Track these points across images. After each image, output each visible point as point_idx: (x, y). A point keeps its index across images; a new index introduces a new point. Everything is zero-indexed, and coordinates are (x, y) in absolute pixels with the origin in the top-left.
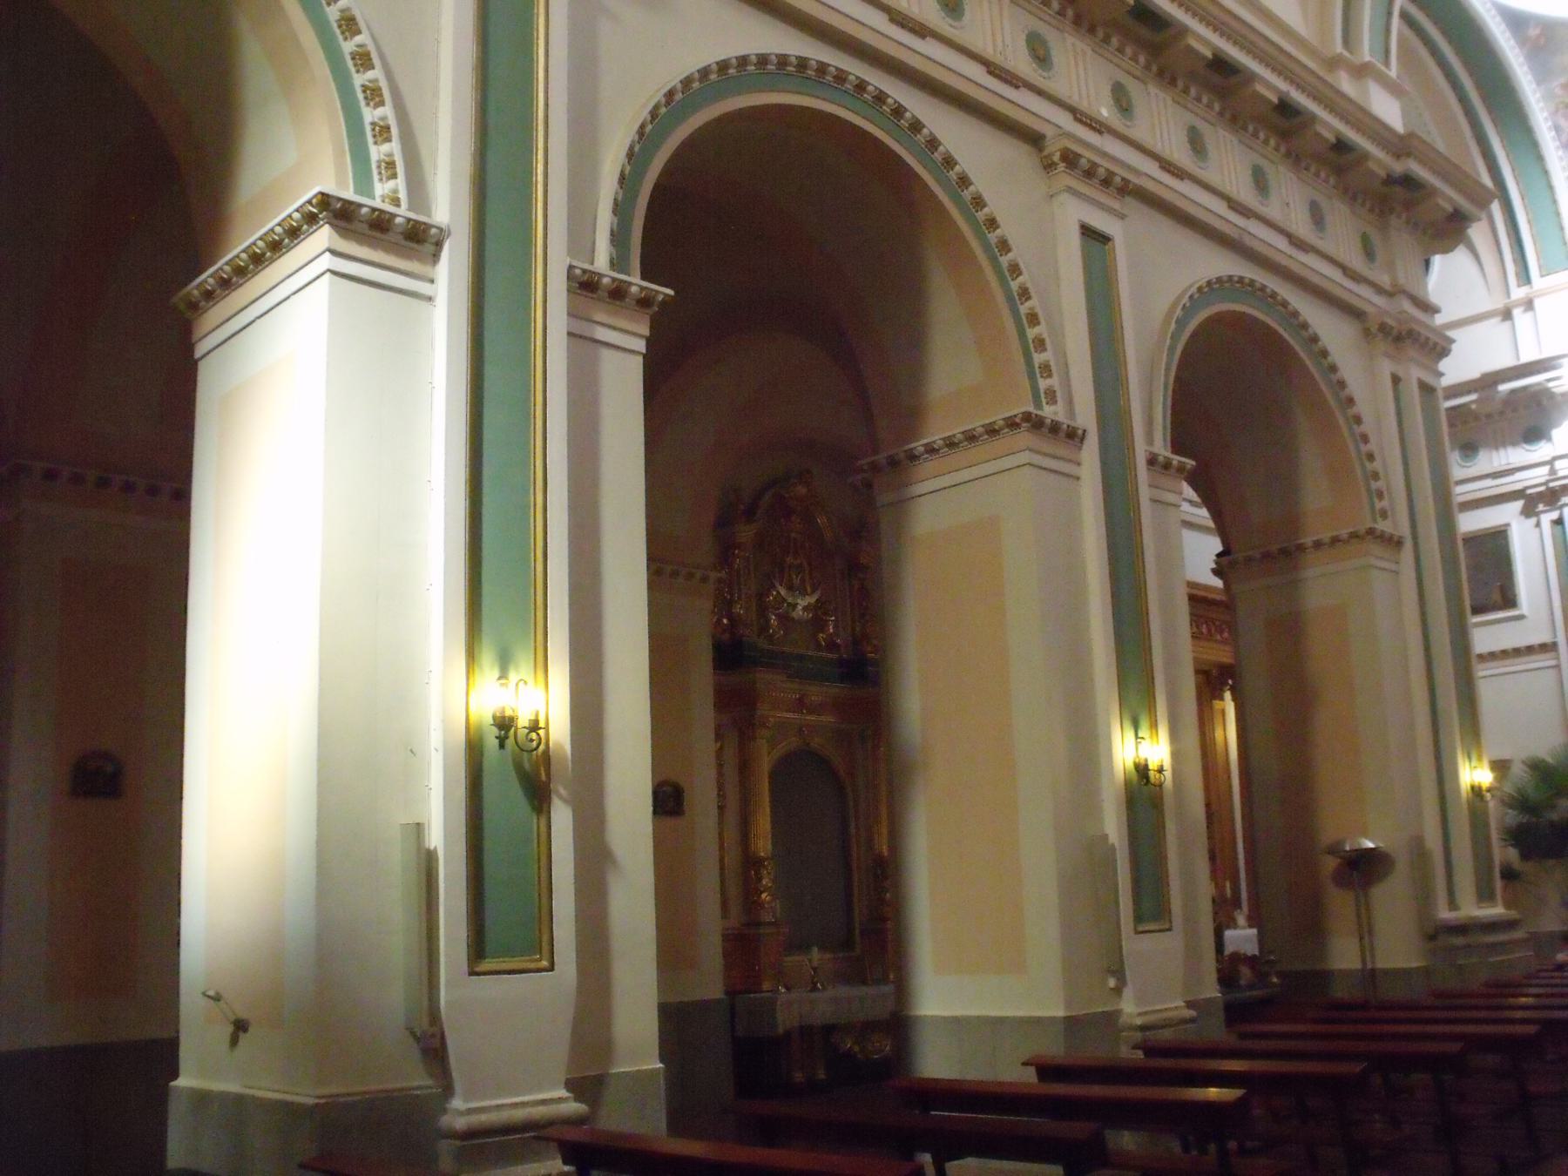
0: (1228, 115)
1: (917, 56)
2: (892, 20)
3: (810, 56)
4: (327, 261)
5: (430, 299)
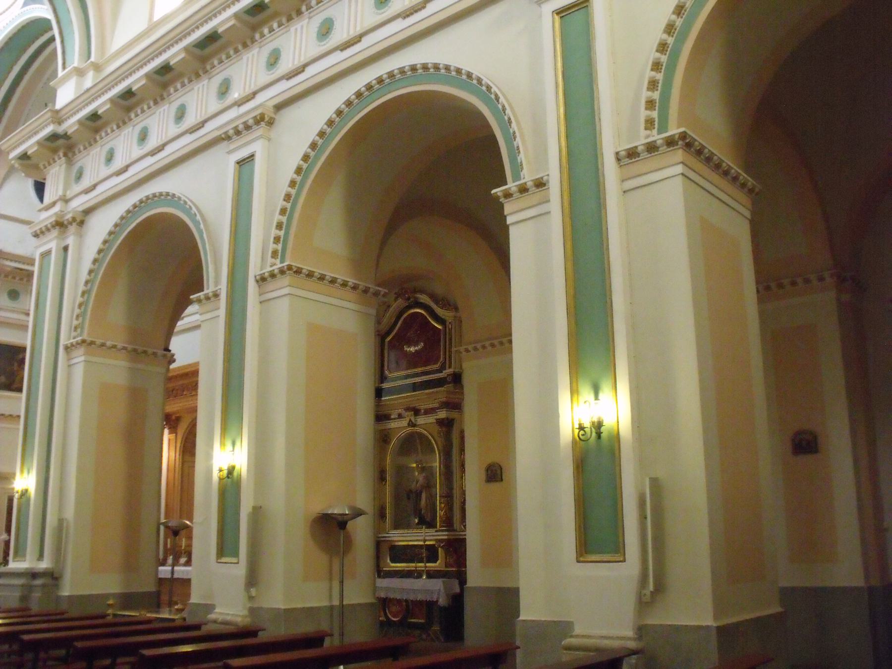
0: (193, 78)
1: (448, 9)
2: (152, 155)
3: (359, 88)
4: (679, 169)
5: (548, 213)
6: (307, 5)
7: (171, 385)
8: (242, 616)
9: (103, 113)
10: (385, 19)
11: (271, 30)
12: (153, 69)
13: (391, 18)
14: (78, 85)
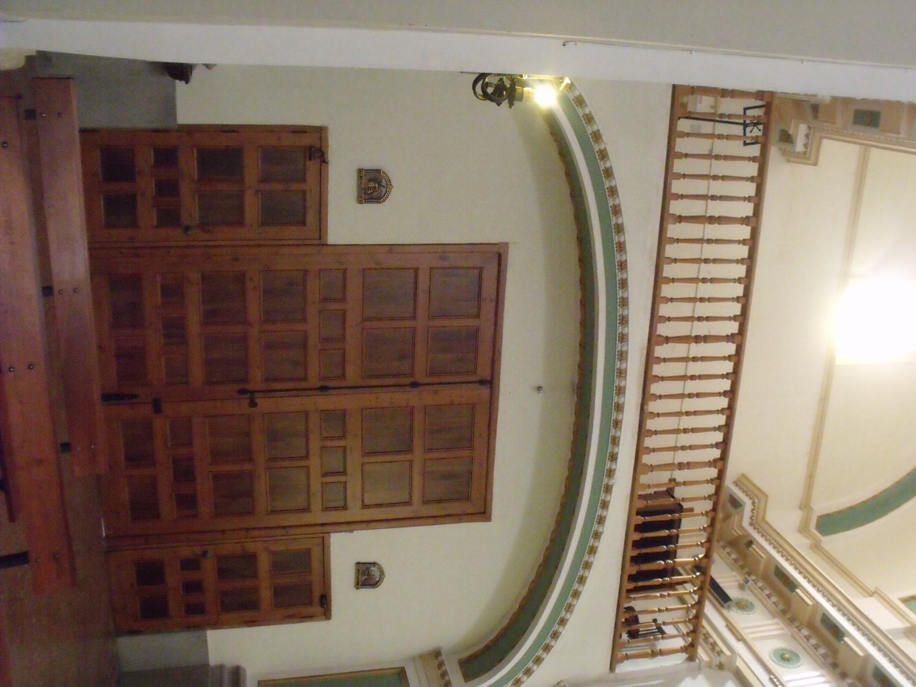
6: (770, 594)
7: (145, 159)
8: (213, 67)
9: (797, 594)
11: (769, 596)
14: (895, 632)
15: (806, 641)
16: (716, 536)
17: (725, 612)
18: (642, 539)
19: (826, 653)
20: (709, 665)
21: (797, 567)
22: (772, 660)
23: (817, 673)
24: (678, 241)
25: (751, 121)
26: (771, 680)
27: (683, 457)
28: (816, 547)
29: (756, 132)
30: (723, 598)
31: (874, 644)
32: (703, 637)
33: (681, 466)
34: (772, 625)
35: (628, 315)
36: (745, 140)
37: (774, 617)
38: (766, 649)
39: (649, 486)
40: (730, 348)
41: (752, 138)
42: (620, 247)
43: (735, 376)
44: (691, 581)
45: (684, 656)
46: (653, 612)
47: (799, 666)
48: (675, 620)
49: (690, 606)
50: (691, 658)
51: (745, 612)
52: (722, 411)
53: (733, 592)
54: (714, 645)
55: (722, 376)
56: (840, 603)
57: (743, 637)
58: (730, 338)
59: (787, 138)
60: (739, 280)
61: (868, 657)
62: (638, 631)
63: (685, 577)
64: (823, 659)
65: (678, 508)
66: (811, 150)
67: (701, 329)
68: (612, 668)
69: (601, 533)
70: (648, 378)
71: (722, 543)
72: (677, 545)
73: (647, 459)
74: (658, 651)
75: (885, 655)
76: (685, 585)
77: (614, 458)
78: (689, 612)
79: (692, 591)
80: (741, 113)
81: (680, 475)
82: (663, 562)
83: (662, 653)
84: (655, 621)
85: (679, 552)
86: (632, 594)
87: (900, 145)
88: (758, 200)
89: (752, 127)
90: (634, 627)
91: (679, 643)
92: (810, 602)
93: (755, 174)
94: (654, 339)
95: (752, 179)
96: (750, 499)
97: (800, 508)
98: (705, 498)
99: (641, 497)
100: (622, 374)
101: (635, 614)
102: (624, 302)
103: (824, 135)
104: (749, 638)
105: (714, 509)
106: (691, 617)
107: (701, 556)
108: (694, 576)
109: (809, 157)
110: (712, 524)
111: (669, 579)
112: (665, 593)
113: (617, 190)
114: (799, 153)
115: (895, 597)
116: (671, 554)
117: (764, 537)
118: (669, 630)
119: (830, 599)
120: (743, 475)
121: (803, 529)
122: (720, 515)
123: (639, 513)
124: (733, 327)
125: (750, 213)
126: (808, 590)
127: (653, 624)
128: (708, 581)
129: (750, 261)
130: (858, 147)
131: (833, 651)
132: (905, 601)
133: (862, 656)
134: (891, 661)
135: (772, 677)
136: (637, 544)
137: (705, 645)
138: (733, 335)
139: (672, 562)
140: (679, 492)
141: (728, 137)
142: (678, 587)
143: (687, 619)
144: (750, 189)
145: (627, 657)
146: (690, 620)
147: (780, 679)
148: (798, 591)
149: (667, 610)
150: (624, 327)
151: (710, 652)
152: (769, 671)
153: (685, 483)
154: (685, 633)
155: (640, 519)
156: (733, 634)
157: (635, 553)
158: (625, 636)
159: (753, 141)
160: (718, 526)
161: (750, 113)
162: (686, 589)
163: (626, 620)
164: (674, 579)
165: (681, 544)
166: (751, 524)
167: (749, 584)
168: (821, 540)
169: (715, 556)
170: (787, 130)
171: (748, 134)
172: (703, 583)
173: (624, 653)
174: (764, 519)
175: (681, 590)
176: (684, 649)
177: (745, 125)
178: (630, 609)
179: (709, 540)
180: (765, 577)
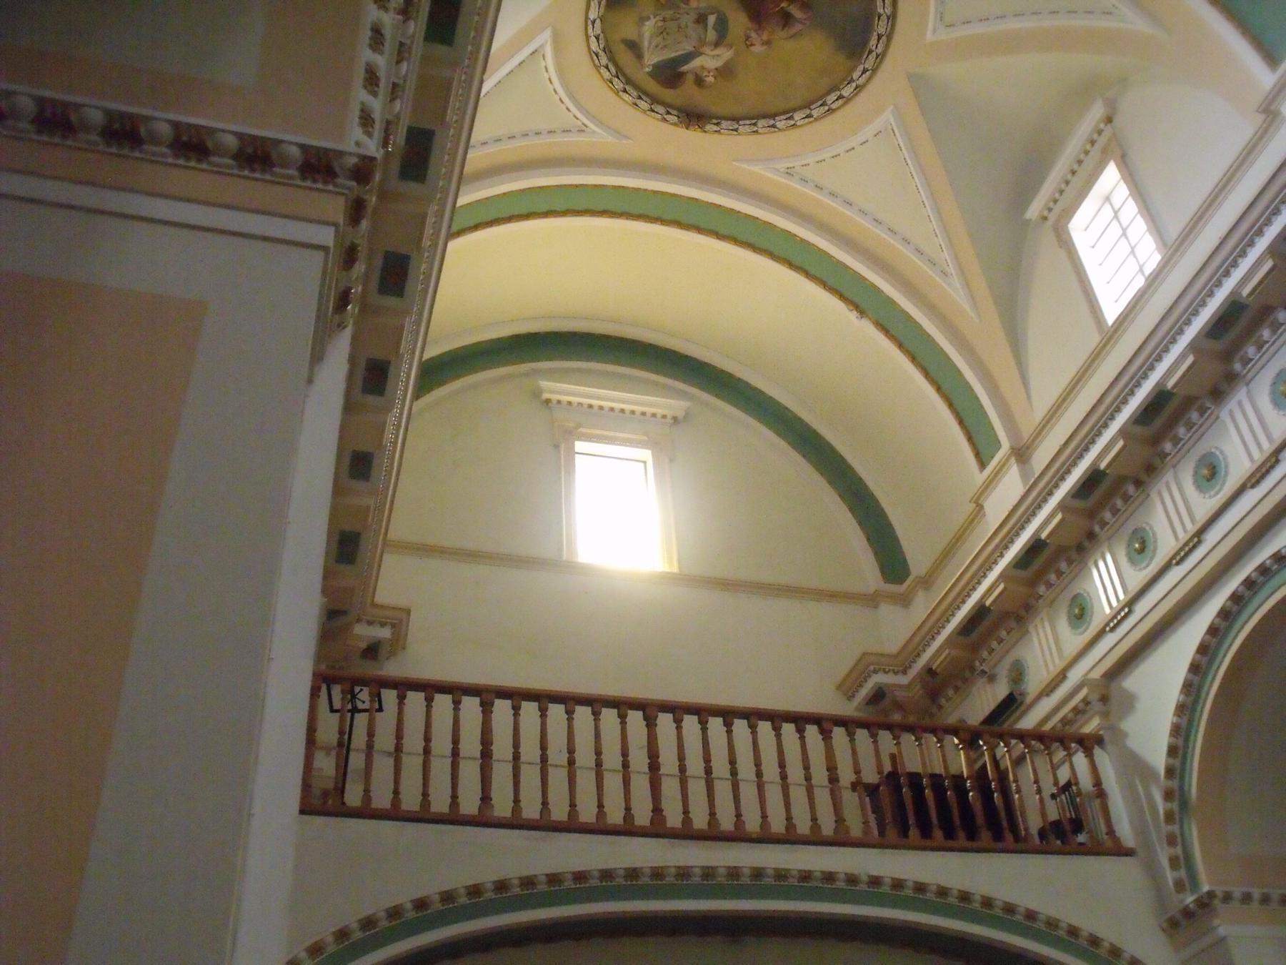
9: (1175, 386)
10: (1224, 500)
12: (1130, 417)
13: (1157, 573)
14: (1024, 476)
15: (1053, 587)
16: (927, 721)
17: (1029, 699)
18: (941, 827)
19: (1066, 560)
20: (1105, 715)
21: (971, 588)
22: (1220, 490)
23: (1035, 640)
24: (517, 801)
25: (349, 702)
26: (1113, 630)
27: (820, 775)
28: (926, 582)
29: (364, 695)
30: (1010, 704)
31: (1045, 500)
32: (1067, 727)
33: (833, 779)
34: (1038, 634)
35: (625, 869)
36: (374, 710)
37: (1027, 632)
38: (1072, 640)
39: (866, 823)
40: (665, 721)
41: (372, 701)
42: (528, 884)
43: (702, 712)
44: (992, 750)
45: (1097, 751)
46: (1041, 800)
47: (1088, 594)
48: (1049, 767)
49: (1027, 750)
50: (1099, 741)
51: (1026, 672)
52: (753, 728)
53: (1001, 691)
54: (1077, 711)
55: (704, 730)
56: (997, 546)
57: (1060, 672)
58: (650, 723)
59: (372, 651)
60: (570, 713)
61: (1062, 506)
62: (1072, 821)
63: (987, 757)
64: (1075, 564)
65: (893, 777)
66: (388, 618)
67: (639, 760)
68: (1129, 853)
69: (939, 886)
70: (713, 835)
71: (934, 710)
72: (944, 775)
73: (828, 828)
74: (1095, 788)
75: (1056, 486)
76: (998, 757)
77: (829, 877)
78: (1036, 749)
79: (1006, 749)
80: (338, 715)
81: (846, 776)
82: (971, 794)
83: (1098, 783)
84: (1053, 796)
85: (953, 771)
86: (1021, 833)
87: (388, 488)
88: (457, 691)
89: (357, 700)
90: (1068, 827)
91: (1080, 759)
92: (1002, 587)
93: (421, 695)
94: (657, 829)
95: (429, 700)
96: (869, 676)
97: (876, 607)
98: (875, 742)
99: (882, 833)
100: (708, 873)
101: (1048, 827)
102: (607, 874)
103: (369, 601)
104: (1060, 664)
105: (889, 727)
106: (1042, 747)
107: (956, 741)
108: (985, 748)
109: (398, 621)
110: (910, 729)
111: (993, 783)
112: (1014, 786)
113: (446, 892)
114: (393, 634)
115: (980, 477)
116: (958, 780)
117: (921, 654)
118: (1064, 775)
119: (993, 561)
120: (839, 687)
121: (904, 601)
122: (897, 717)
123: (904, 832)
124: (635, 717)
125: (476, 701)
126: (1042, 522)
127: (1058, 799)
128: (987, 727)
129: (543, 699)
130: (386, 557)
131: (1061, 551)
132: (982, 465)
133: (1194, 356)
134: (1062, 479)
135: (1108, 629)
136: (950, 834)
137: (1078, 724)
138: (646, 718)
139: (969, 781)
140: (870, 777)
141: (371, 735)
142: (1002, 766)
143: (1046, 752)
144: (443, 702)
145: (1111, 832)
146: (1047, 748)
147: (1109, 618)
148: (988, 603)
149: (1036, 782)
150: (642, 873)
151: (1087, 716)
152: (1101, 634)
153: (857, 772)
154: (1065, 753)
155: (914, 832)
156: (1268, 472)
157: (961, 834)
158: (1081, 838)
159: (376, 699)
160: (911, 719)
161: (337, 704)
162: (1004, 756)
163: (1058, 838)
164: (992, 775)
165: (943, 770)
166: (904, 672)
167: (986, 669)
168: (917, 577)
169: (952, 720)
170: (362, 650)
171: (367, 706)
172: (993, 735)
173: (1106, 837)
174: (896, 656)
175: (1007, 763)
176: (1089, 754)
177: (355, 710)
178: (1042, 834)
179: (934, 731)
180: (975, 648)
